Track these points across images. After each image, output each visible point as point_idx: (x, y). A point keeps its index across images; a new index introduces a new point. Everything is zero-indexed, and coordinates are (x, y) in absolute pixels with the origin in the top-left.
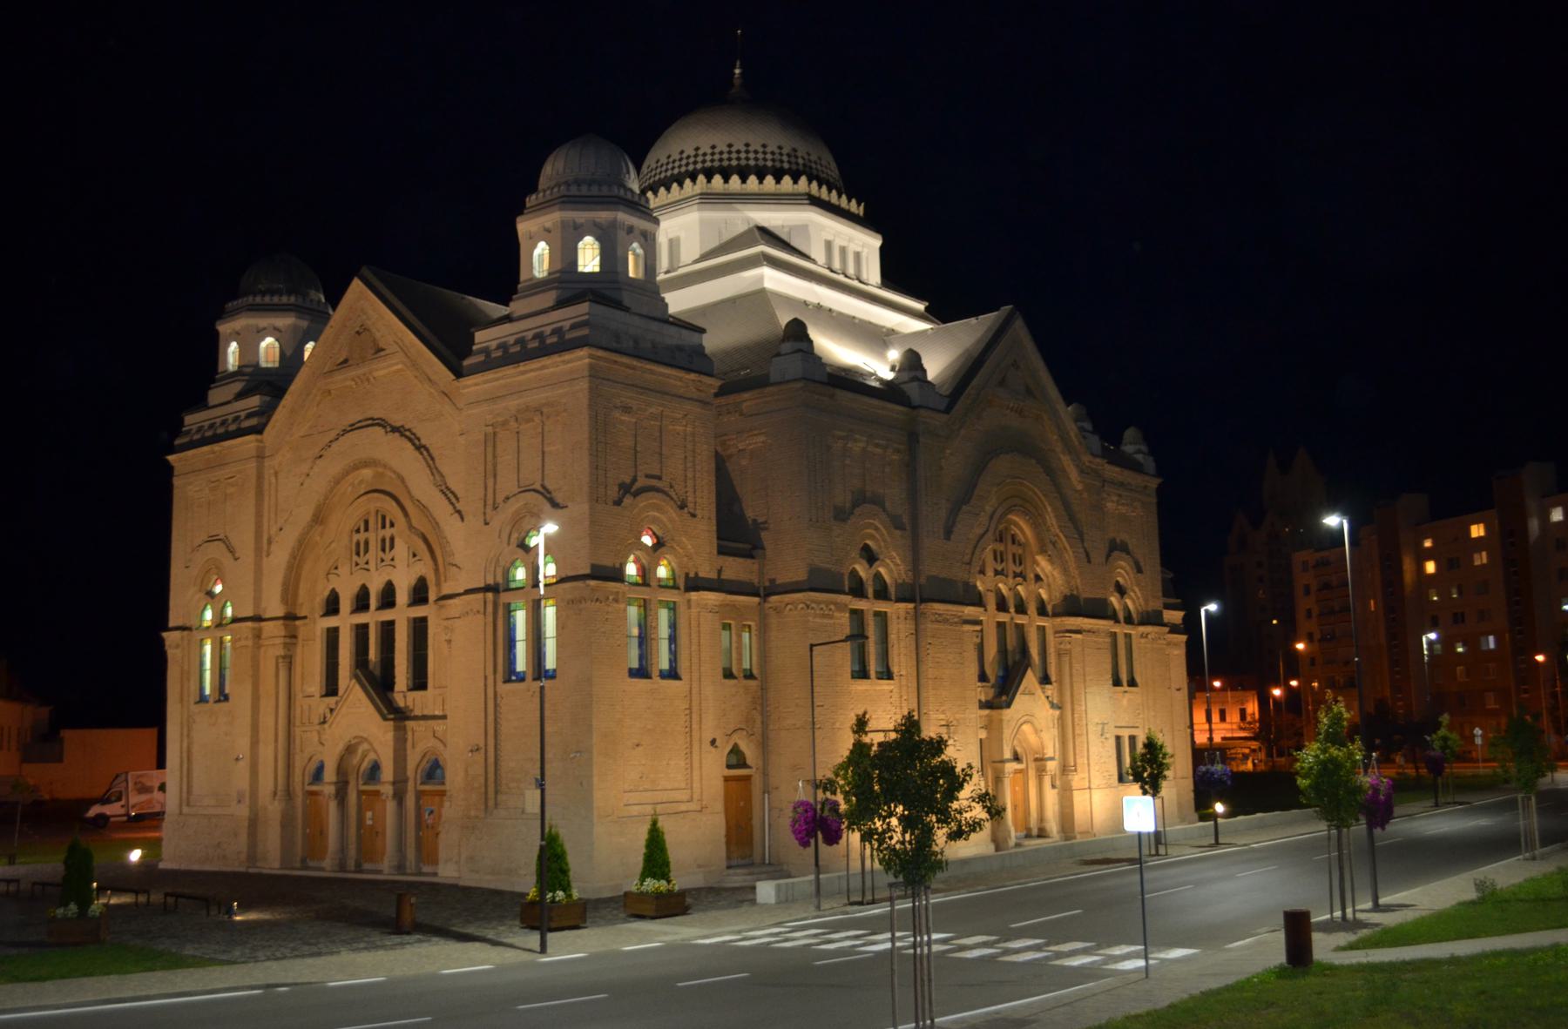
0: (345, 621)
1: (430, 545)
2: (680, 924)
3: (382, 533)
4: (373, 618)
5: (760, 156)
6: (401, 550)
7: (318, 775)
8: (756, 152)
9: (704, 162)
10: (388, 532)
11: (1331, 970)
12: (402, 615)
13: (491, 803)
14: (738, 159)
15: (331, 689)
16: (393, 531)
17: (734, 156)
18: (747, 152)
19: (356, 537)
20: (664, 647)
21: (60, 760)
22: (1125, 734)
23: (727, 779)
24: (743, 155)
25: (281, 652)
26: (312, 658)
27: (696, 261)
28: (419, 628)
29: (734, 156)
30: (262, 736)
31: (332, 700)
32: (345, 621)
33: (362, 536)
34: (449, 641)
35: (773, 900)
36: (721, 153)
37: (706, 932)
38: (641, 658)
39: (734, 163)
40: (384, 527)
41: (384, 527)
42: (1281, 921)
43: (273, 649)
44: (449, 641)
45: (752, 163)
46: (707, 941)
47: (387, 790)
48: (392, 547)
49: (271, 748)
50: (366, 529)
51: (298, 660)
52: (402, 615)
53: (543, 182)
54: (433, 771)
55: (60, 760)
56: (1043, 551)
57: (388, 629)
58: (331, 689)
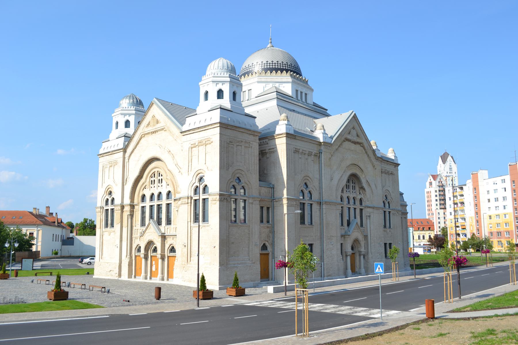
0: (147, 204)
2: (242, 299)
3: (159, 178)
4: (155, 203)
7: (139, 250)
10: (160, 178)
12: (164, 202)
16: (162, 177)
17: (274, 65)
19: (151, 179)
20: (242, 212)
21: (73, 245)
22: (388, 242)
23: (261, 254)
29: (274, 65)
32: (147, 204)
33: (153, 179)
34: (177, 211)
35: (272, 292)
37: (249, 302)
46: (249, 305)
47: (159, 256)
48: (162, 182)
50: (154, 177)
52: (164, 202)
53: (208, 72)
54: (173, 250)
55: (73, 245)
56: (266, 138)
58: (143, 224)
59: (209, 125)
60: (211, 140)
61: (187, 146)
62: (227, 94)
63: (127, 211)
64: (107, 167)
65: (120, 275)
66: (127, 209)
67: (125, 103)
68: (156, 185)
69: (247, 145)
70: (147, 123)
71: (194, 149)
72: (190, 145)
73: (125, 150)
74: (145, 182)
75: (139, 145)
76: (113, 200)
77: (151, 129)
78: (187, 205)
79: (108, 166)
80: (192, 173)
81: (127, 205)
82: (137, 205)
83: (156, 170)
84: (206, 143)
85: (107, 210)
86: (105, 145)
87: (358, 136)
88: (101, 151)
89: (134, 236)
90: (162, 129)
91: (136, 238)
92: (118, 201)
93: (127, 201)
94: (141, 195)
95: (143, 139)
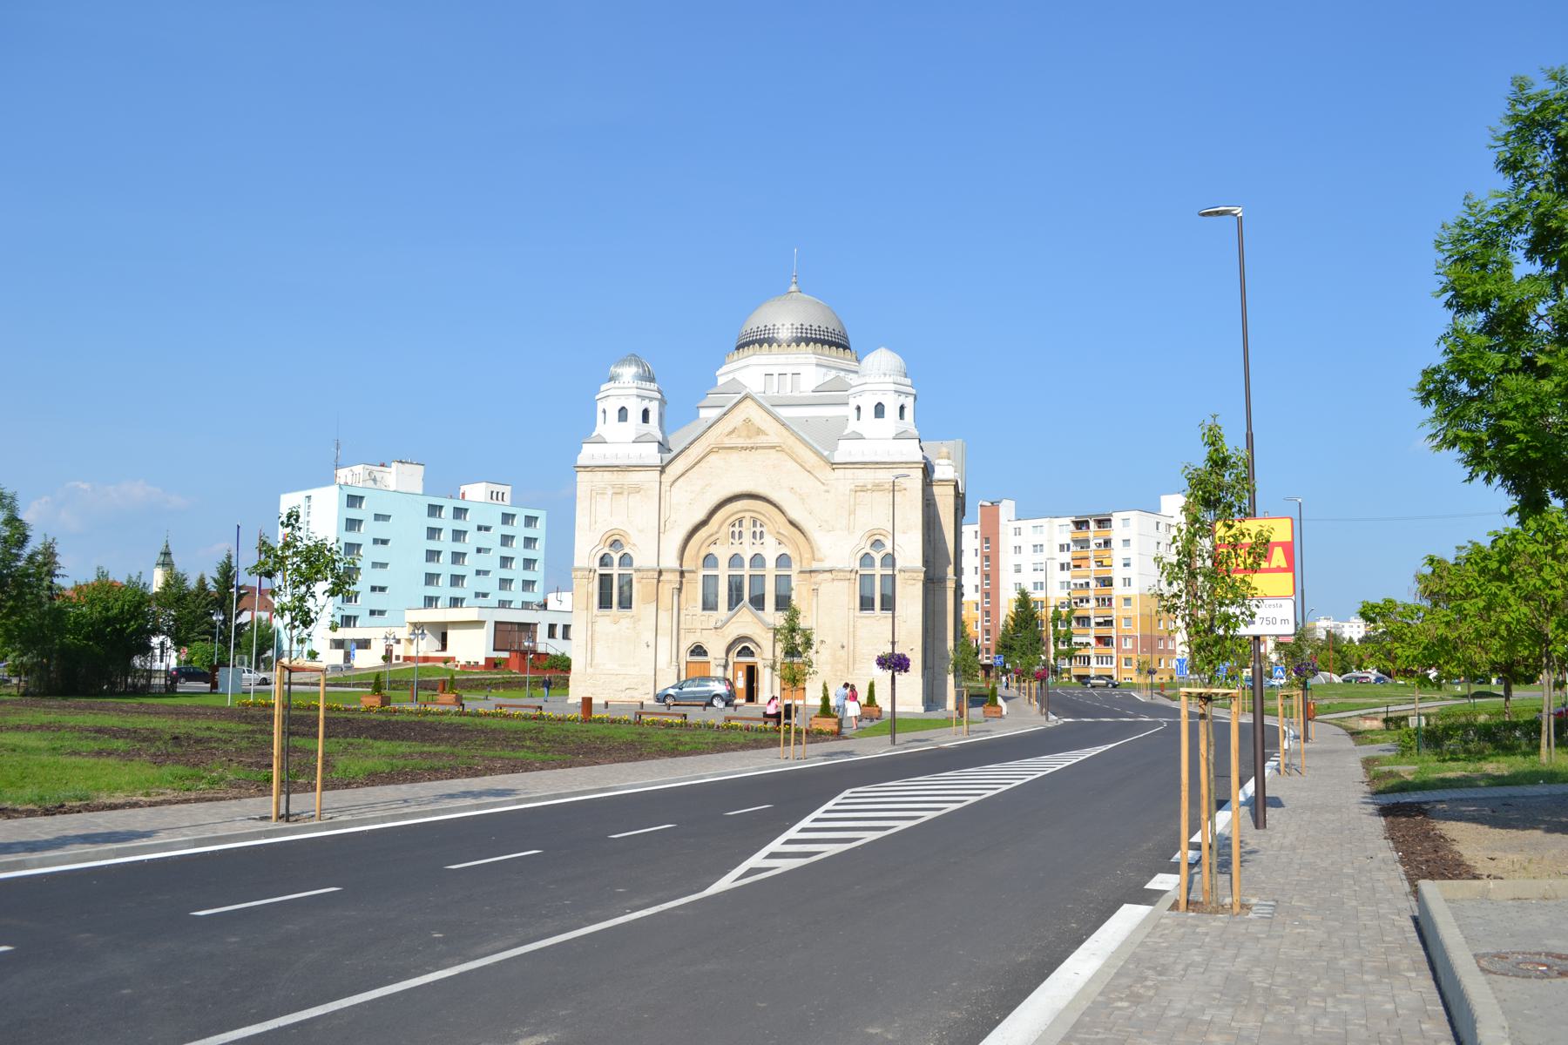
6: (769, 539)
26: (695, 591)
58: (709, 605)
66: (671, 579)
67: (628, 372)
70: (730, 429)
77: (740, 442)
81: (673, 571)
83: (747, 515)
88: (582, 460)
91: (689, 630)
93: (670, 561)
94: (703, 554)
95: (712, 457)
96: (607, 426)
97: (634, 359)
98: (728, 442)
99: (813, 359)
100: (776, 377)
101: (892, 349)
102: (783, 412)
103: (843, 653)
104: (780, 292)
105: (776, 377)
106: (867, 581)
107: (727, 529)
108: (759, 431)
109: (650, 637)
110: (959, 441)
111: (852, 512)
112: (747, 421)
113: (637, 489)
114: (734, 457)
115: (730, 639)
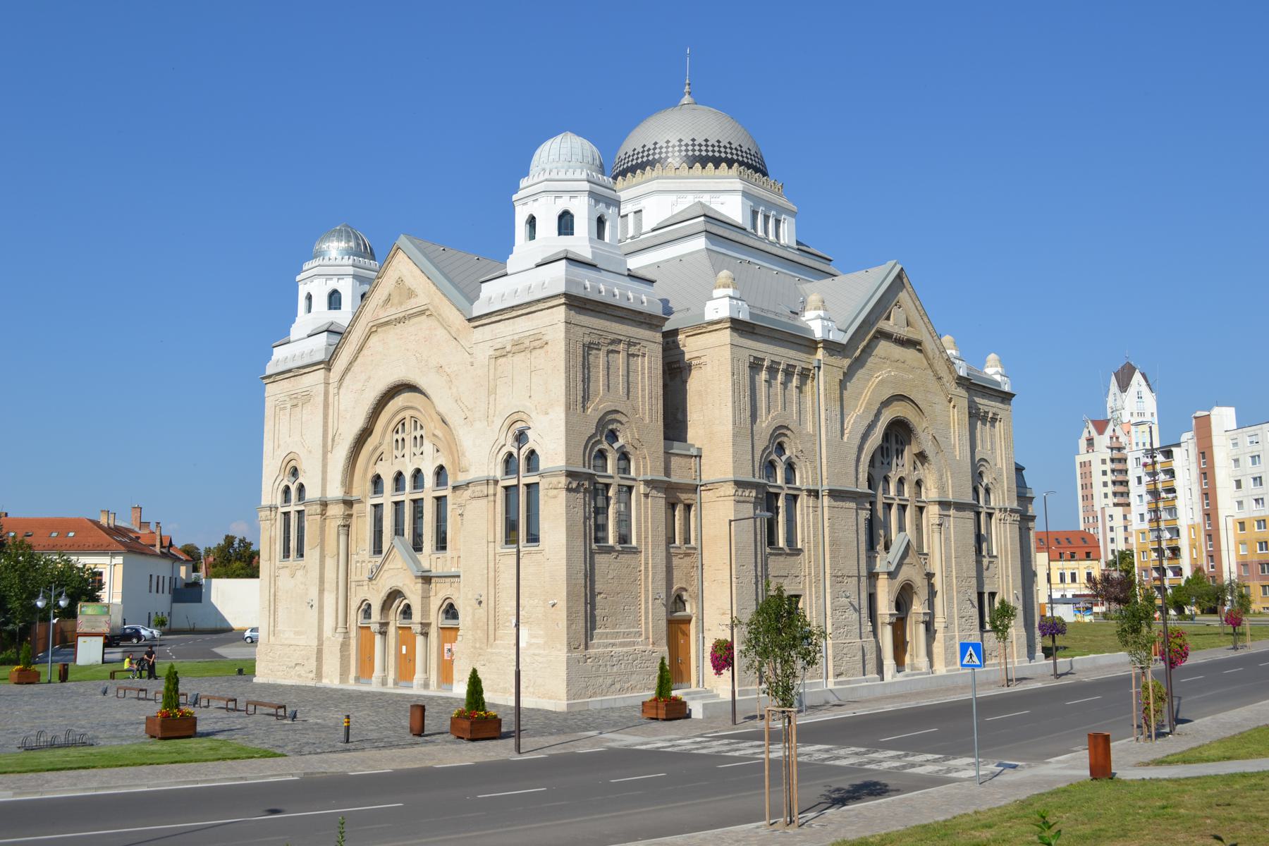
0: (387, 498)
1: (451, 444)
4: (407, 496)
5: (703, 148)
6: (428, 447)
8: (700, 145)
9: (660, 153)
11: (1124, 783)
13: (491, 637)
14: (700, 150)
15: (378, 549)
16: (422, 432)
17: (697, 148)
18: (694, 145)
24: (703, 148)
25: (340, 522)
26: (363, 528)
27: (654, 230)
28: (440, 500)
30: (327, 586)
31: (379, 559)
32: (387, 498)
36: (687, 145)
38: (555, 476)
39: (710, 154)
40: (416, 428)
41: (416, 428)
42: (1086, 739)
43: (333, 525)
44: (461, 515)
45: (723, 155)
46: (644, 747)
49: (333, 596)
50: (403, 430)
51: (353, 529)
57: (417, 503)
58: (378, 549)
59: (539, 301)
60: (546, 338)
61: (483, 353)
62: (582, 225)
63: (335, 517)
64: (285, 408)
65: (319, 675)
68: (406, 451)
69: (633, 350)
70: (384, 298)
71: (501, 360)
72: (492, 352)
73: (328, 364)
74: (381, 444)
75: (365, 352)
76: (301, 488)
77: (392, 312)
78: (485, 500)
79: (289, 406)
80: (498, 422)
81: (337, 501)
82: (359, 501)
83: (407, 414)
84: (537, 343)
85: (287, 514)
86: (279, 353)
87: (388, 300)
88: (270, 369)
89: (353, 577)
90: (422, 313)
91: (359, 584)
92: (312, 493)
93: (335, 491)
94: (370, 475)
95: (374, 339)
96: (523, 251)
97: (348, 234)
98: (384, 315)
99: (738, 184)
100: (631, 216)
101: (579, 134)
102: (634, 263)
103: (481, 611)
104: (671, 102)
105: (631, 216)
106: (512, 492)
107: (390, 437)
108: (411, 294)
109: (314, 593)
110: (403, 241)
111: (492, 392)
112: (400, 281)
113: (307, 397)
114: (390, 334)
115: (383, 594)
